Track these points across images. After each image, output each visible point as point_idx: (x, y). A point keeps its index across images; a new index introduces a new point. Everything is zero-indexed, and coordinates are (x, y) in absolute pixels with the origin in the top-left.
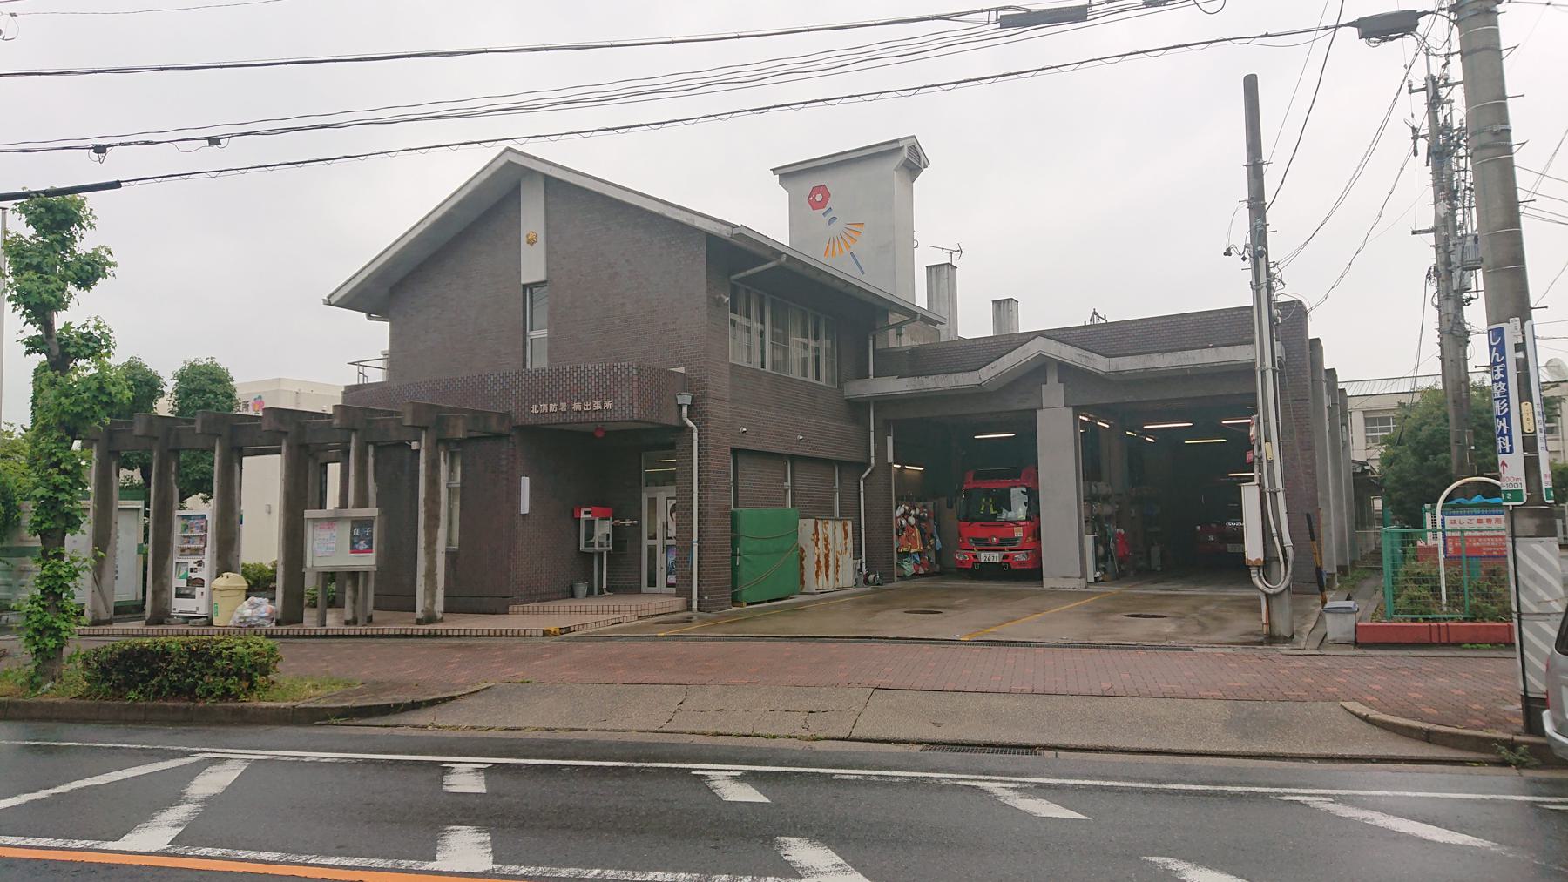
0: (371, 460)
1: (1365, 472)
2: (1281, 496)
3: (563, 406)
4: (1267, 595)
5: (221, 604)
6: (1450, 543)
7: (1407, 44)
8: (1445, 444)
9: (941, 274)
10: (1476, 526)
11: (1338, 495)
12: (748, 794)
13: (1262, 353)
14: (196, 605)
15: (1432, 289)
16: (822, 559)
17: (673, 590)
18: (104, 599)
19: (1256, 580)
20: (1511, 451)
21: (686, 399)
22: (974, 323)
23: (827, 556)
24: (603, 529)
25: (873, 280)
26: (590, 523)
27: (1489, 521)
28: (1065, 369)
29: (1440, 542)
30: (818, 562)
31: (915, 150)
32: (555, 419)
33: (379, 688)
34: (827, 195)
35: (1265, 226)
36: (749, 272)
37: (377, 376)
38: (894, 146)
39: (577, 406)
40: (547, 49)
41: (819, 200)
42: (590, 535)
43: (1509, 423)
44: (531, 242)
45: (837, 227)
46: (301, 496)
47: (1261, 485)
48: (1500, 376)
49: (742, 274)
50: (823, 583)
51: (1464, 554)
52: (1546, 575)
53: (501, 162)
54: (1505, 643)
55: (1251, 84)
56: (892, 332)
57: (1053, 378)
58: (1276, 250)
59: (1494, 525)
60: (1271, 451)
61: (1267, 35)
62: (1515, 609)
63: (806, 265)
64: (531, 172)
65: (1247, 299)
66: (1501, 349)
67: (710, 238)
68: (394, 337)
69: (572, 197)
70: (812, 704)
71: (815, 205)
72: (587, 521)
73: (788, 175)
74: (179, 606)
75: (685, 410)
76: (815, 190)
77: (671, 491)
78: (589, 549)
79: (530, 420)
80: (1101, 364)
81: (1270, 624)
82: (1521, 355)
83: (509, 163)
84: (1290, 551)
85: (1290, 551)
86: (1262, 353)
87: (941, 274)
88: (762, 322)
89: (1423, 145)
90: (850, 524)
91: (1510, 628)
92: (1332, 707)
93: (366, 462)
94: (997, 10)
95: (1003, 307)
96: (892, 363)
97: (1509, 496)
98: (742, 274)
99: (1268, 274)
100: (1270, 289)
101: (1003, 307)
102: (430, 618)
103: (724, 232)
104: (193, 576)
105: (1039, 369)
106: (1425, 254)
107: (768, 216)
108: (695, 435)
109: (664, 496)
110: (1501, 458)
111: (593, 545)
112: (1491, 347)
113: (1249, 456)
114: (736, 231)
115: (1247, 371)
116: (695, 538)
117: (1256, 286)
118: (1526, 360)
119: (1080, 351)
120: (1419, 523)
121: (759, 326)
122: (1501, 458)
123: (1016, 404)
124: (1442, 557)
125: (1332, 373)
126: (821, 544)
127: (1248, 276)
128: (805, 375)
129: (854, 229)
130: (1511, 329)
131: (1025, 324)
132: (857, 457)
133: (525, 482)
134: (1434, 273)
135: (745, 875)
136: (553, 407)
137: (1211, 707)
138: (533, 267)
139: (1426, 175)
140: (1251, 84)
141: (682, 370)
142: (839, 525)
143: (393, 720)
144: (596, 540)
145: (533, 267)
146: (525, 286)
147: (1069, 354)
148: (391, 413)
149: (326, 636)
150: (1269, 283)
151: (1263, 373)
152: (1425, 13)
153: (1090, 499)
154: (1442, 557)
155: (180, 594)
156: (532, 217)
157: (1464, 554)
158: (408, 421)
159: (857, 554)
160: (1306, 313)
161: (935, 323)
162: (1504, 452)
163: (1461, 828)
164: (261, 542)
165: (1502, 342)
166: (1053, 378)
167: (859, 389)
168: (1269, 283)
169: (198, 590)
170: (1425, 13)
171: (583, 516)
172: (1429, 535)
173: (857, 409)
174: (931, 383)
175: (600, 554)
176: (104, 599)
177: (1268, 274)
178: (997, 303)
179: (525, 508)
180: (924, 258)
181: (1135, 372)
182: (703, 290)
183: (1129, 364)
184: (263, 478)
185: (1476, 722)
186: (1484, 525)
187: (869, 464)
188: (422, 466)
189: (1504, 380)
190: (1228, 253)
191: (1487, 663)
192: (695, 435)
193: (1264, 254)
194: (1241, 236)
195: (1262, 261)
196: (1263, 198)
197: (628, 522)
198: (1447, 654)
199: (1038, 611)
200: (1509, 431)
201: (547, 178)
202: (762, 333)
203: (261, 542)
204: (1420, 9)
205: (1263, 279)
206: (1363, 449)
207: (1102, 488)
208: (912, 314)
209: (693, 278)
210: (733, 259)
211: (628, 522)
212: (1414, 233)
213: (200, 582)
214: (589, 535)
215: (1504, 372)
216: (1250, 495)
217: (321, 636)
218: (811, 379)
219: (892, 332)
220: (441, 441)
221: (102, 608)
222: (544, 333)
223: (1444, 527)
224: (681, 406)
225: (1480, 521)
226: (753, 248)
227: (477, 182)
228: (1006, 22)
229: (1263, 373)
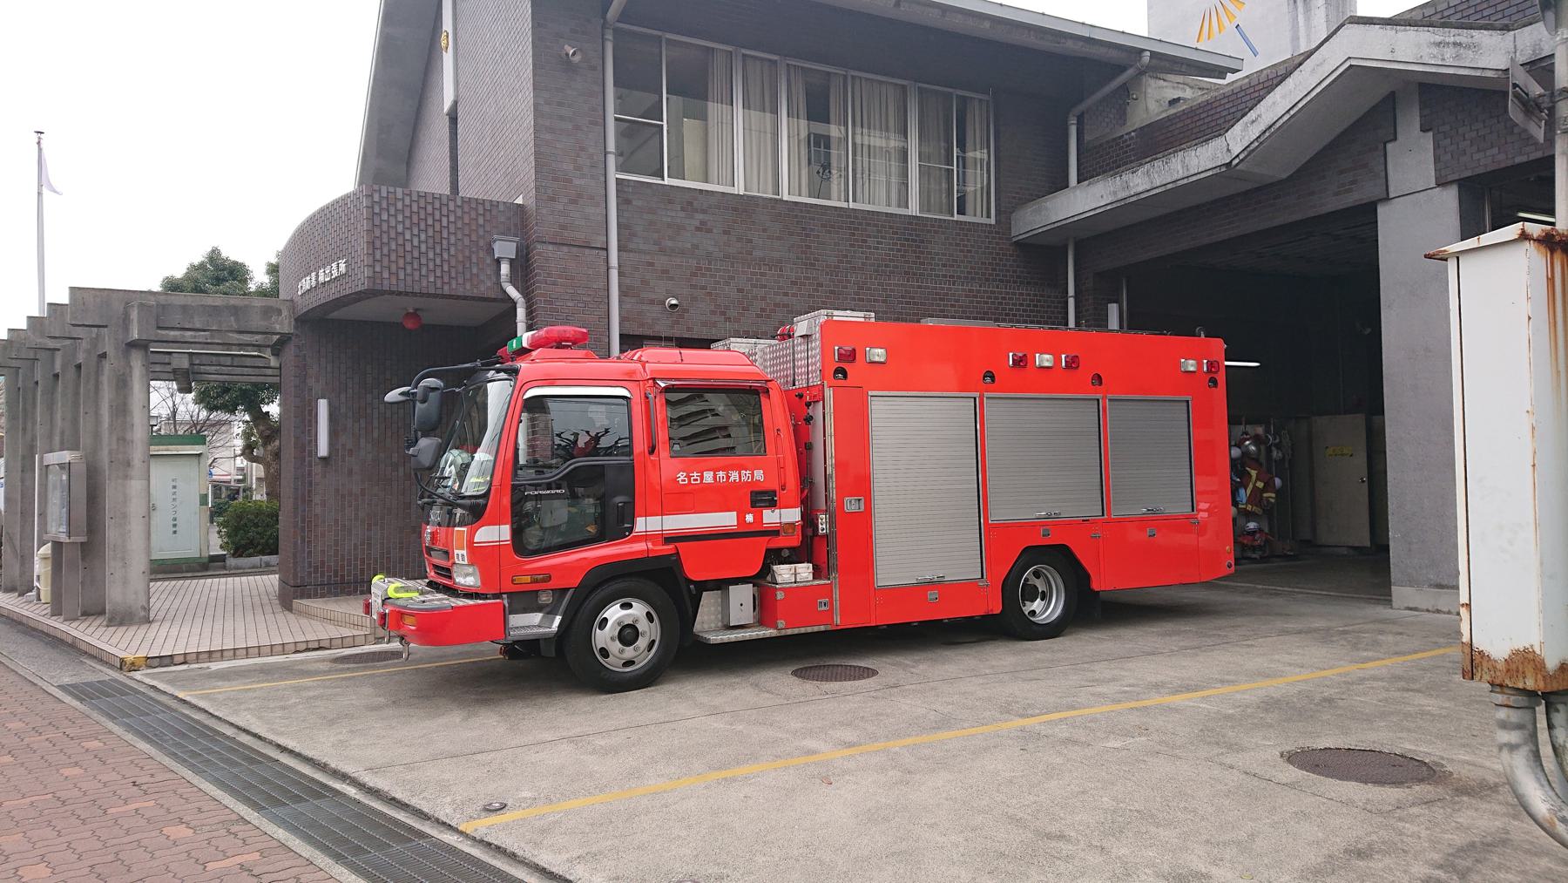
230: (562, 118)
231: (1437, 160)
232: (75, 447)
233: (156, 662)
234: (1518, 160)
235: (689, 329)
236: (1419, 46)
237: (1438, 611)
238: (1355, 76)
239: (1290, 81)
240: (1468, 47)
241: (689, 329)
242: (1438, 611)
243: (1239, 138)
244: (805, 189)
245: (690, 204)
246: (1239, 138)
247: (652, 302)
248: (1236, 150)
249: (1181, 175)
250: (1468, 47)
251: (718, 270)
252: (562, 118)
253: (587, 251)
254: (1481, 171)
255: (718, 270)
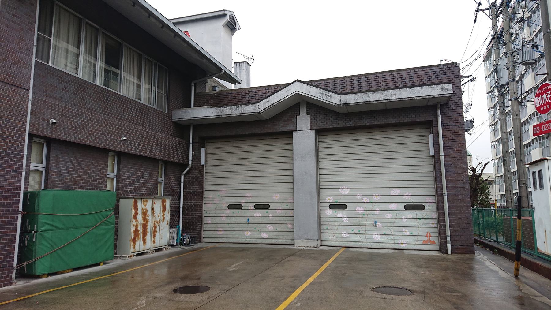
16: (140, 228)
23: (145, 226)
30: (136, 231)
50: (140, 246)
80: (335, 99)
88: (78, 47)
90: (168, 203)
96: (203, 100)
119: (322, 91)
121: (75, 50)
126: (139, 217)
132: (182, 161)
135: (516, 253)
142: (158, 203)
147: (315, 93)
159: (173, 223)
163: (42, 151)
174: (228, 111)
181: (356, 105)
183: (352, 99)
187: (187, 165)
202: (78, 56)
230: (14, 22)
231: (311, 123)
232: (43, 144)
233: (440, 198)
234: (331, 127)
235: (59, 135)
236: (316, 92)
237: (308, 247)
238: (298, 96)
239: (279, 93)
240: (329, 96)
241: (59, 135)
242: (308, 247)
243: (263, 105)
244: (103, 84)
245: (61, 78)
246: (263, 105)
247: (44, 120)
248: (262, 109)
249: (243, 112)
250: (329, 96)
251: (74, 110)
252: (14, 22)
253: (20, 89)
254: (321, 128)
255: (74, 110)
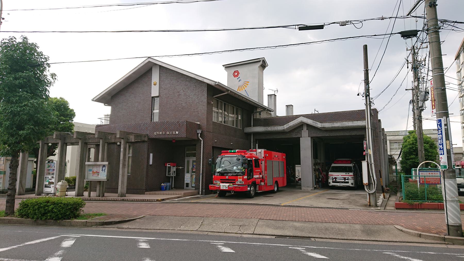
0: (106, 147)
1: (392, 158)
2: (373, 165)
3: (164, 133)
4: (369, 194)
5: (53, 188)
6: (421, 180)
7: (415, 39)
8: (419, 150)
9: (272, 97)
10: (429, 175)
11: (385, 164)
12: (226, 250)
13: (367, 123)
14: (51, 190)
15: (411, 107)
17: (194, 188)
18: (22, 188)
19: (366, 189)
20: (443, 154)
21: (199, 131)
22: (281, 112)
24: (174, 169)
25: (254, 98)
26: (170, 168)
27: (435, 174)
28: (308, 126)
29: (418, 179)
31: (264, 61)
32: (161, 137)
33: (112, 216)
34: (238, 73)
35: (369, 87)
36: (219, 95)
37: (104, 122)
38: (259, 60)
39: (168, 133)
40: (168, 31)
41: (236, 74)
42: (169, 171)
43: (443, 146)
44: (155, 85)
45: (241, 83)
46: (84, 157)
47: (367, 162)
48: (440, 133)
49: (217, 96)
51: (425, 183)
52: (448, 188)
53: (147, 61)
54: (441, 208)
55: (365, 47)
56: (258, 113)
57: (305, 128)
58: (372, 94)
59: (436, 175)
60: (370, 152)
61: (375, 35)
62: (444, 199)
63: (235, 94)
64: (156, 64)
65: (364, 108)
66: (441, 125)
67: (209, 85)
68: (113, 111)
69: (165, 71)
70: (241, 223)
71: (235, 76)
72: (169, 167)
73: (227, 67)
74: (47, 190)
75: (199, 135)
76: (235, 72)
77: (194, 159)
78: (169, 176)
79: (154, 137)
80: (319, 125)
81: (370, 202)
82: (446, 127)
83: (149, 62)
84: (376, 181)
85: (376, 181)
86: (367, 123)
87: (272, 97)
89: (410, 66)
91: (443, 205)
92: (392, 227)
93: (104, 148)
94: (298, 25)
95: (289, 107)
96: (258, 122)
97: (443, 167)
98: (217, 96)
99: (370, 101)
100: (370, 105)
101: (289, 107)
102: (122, 195)
103: (213, 84)
104: (50, 181)
105: (301, 126)
106: (409, 96)
107: (221, 78)
108: (202, 142)
109: (192, 159)
110: (440, 156)
111: (170, 174)
112: (438, 125)
113: (364, 153)
114: (216, 84)
115: (363, 128)
116: (201, 173)
117: (366, 105)
118: (448, 128)
119: (313, 121)
120: (410, 174)
122: (440, 156)
123: (294, 136)
124: (418, 184)
125: (383, 129)
127: (365, 101)
128: (233, 125)
129: (246, 83)
130: (443, 119)
131: (296, 112)
133: (151, 155)
134: (412, 101)
136: (161, 133)
137: (358, 227)
138: (155, 91)
139: (411, 74)
140: (365, 47)
141: (199, 123)
143: (119, 225)
144: (171, 172)
145: (155, 91)
146: (152, 97)
147: (310, 122)
148: (113, 134)
149: (90, 200)
150: (370, 104)
151: (368, 129)
152: (419, 31)
153: (315, 164)
154: (418, 184)
155: (46, 187)
156: (155, 77)
157: (425, 183)
158: (118, 136)
160: (378, 112)
161: (271, 111)
162: (441, 154)
164: (71, 171)
165: (441, 123)
166: (305, 128)
167: (248, 130)
168: (370, 104)
169: (52, 185)
170: (419, 31)
171: (168, 165)
172: (414, 177)
173: (248, 135)
174: (270, 129)
175: (172, 177)
176: (22, 188)
177: (370, 101)
178: (287, 106)
179: (151, 163)
180: (266, 93)
181: (329, 128)
182: (206, 100)
183: (327, 125)
184: (72, 152)
185: (434, 232)
186: (431, 175)
188: (122, 150)
189: (441, 134)
190: (358, 95)
191: (432, 215)
192: (202, 142)
193: (369, 95)
194: (362, 89)
195: (368, 97)
196: (368, 80)
197: (181, 168)
198: (421, 212)
199: (303, 196)
200: (443, 149)
201: (160, 66)
203: (71, 171)
204: (418, 29)
205: (368, 103)
206: (395, 152)
207: (319, 161)
208: (264, 109)
209: (202, 97)
210: (215, 92)
211: (181, 168)
212: (406, 90)
213: (53, 183)
214: (169, 171)
215: (441, 132)
216: (364, 164)
217: (89, 200)
218: (235, 127)
219: (258, 113)
220: (127, 142)
221: (22, 190)
222: (158, 111)
223: (417, 175)
224: (198, 134)
225: (429, 174)
226: (221, 89)
227: (139, 67)
228: (300, 29)
229: (368, 129)
